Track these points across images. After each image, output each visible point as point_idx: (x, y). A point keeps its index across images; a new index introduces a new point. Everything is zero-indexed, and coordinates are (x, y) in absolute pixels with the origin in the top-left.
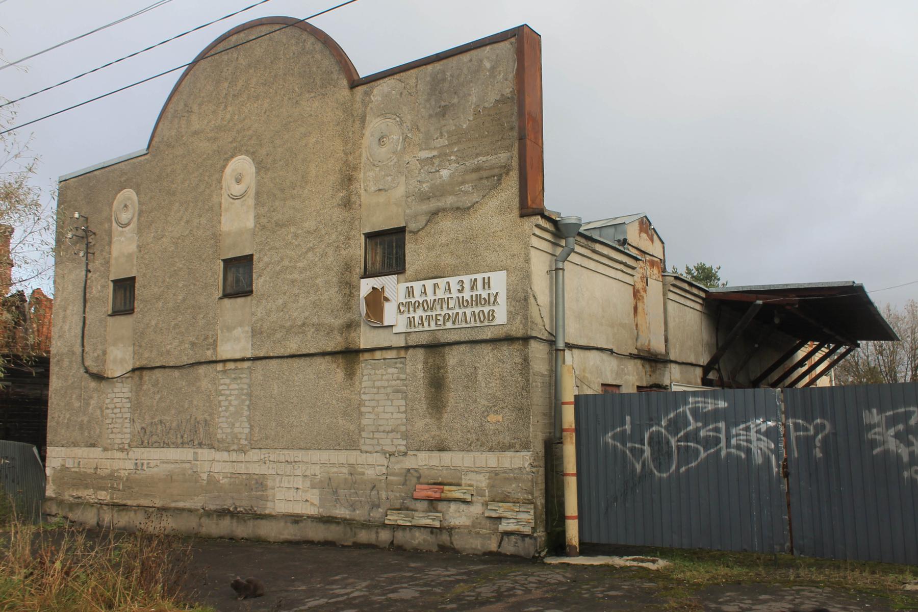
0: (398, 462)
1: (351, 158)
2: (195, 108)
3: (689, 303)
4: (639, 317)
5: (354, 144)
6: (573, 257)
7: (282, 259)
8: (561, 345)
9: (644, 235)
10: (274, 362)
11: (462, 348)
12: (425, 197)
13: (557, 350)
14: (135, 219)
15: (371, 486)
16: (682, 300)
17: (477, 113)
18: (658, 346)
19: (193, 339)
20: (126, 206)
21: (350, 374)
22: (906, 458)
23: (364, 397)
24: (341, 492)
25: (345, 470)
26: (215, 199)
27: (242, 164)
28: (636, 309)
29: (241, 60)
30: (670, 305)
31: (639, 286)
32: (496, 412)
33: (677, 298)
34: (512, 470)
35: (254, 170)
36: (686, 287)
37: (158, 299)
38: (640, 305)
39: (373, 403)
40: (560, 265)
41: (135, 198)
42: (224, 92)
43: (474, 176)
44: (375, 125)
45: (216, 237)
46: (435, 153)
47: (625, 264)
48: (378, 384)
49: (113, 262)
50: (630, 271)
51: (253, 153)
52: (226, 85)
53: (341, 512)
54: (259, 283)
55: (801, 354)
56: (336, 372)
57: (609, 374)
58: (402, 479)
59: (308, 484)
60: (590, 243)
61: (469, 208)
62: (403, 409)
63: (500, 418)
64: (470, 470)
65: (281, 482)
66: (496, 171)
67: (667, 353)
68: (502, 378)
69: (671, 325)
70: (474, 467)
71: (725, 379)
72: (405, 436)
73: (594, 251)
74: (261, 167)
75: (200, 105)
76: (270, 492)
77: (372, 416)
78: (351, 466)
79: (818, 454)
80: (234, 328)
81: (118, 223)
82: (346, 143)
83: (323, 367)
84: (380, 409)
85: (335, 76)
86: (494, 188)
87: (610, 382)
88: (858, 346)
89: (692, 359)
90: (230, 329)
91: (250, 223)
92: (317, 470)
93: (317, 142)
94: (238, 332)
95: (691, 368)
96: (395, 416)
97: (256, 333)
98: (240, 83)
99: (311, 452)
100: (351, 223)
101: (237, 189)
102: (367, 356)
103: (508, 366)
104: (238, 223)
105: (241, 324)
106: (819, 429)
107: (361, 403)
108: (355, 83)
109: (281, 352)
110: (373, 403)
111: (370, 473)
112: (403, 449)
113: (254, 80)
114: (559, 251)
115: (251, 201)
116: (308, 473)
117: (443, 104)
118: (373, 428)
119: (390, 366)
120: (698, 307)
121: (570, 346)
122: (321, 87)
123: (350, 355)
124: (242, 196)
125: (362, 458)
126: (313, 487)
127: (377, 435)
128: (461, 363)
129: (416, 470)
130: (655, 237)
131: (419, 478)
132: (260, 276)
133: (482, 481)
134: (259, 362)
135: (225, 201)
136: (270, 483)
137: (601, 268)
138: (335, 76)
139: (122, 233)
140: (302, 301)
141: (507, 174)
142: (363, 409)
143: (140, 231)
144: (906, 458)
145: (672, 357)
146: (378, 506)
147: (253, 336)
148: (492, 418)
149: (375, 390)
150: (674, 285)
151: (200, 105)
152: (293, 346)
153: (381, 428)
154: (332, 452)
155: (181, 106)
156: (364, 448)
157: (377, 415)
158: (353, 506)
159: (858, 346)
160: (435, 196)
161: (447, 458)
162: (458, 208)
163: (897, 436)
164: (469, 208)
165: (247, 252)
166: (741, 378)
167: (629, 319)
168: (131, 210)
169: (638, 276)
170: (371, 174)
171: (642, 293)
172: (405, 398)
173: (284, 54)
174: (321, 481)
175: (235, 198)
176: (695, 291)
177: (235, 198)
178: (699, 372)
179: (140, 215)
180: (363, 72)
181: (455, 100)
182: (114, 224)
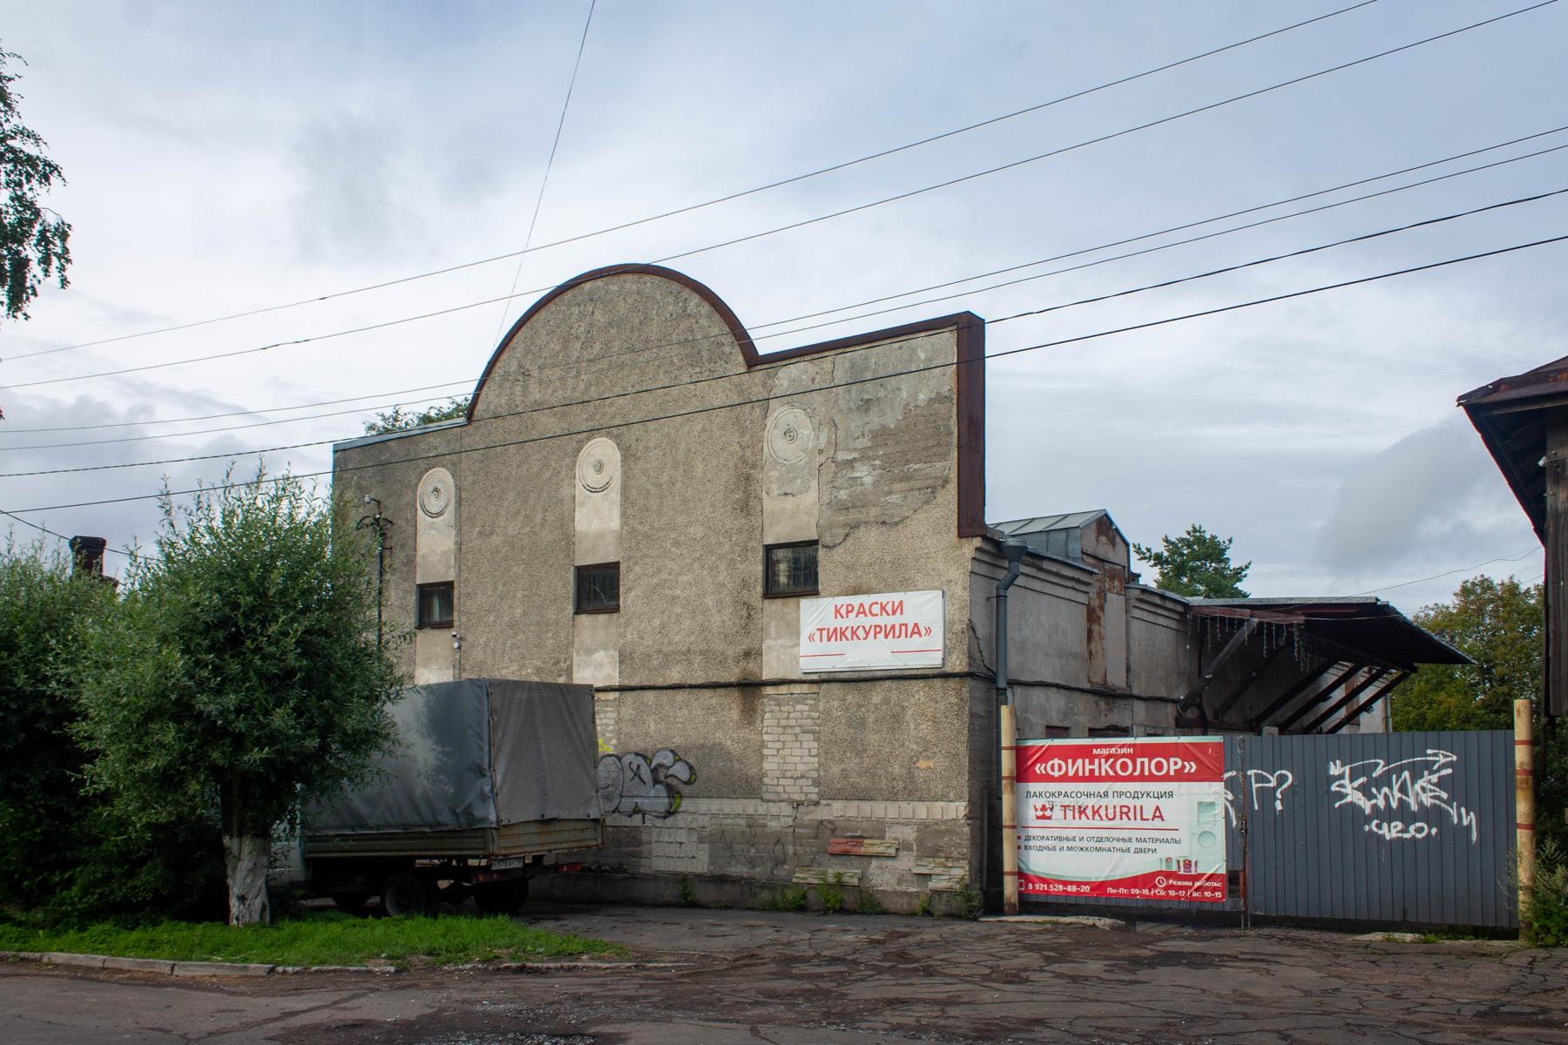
0: (807, 813)
1: (748, 453)
2: (535, 373)
3: (1161, 620)
4: (1093, 644)
5: (752, 436)
6: (1020, 581)
7: (659, 570)
8: (1002, 684)
9: (1103, 539)
10: (650, 695)
11: (887, 683)
12: (845, 508)
13: (998, 689)
14: (451, 508)
15: (774, 840)
16: (1151, 618)
17: (906, 413)
18: (1117, 679)
19: (538, 663)
20: (436, 490)
21: (750, 713)
22: (1368, 811)
23: (765, 737)
24: (737, 847)
25: (743, 822)
26: (565, 491)
27: (602, 449)
28: (1090, 633)
29: (598, 316)
30: (1136, 626)
31: (1095, 603)
32: (928, 758)
33: (1145, 615)
34: (945, 822)
35: (618, 456)
36: (1158, 601)
37: (489, 612)
38: (1095, 628)
39: (778, 745)
40: (1002, 593)
41: (451, 481)
42: (576, 354)
43: (904, 485)
44: (782, 415)
45: (568, 539)
46: (856, 455)
47: (1078, 581)
48: (784, 722)
49: (419, 560)
50: (1083, 588)
51: (618, 436)
52: (578, 345)
53: (738, 870)
54: (627, 599)
55: (1331, 677)
56: (730, 707)
57: (1054, 715)
58: (813, 832)
59: (695, 837)
60: (1037, 562)
61: (897, 524)
62: (814, 752)
63: (931, 764)
64: (895, 823)
65: (659, 835)
66: (930, 482)
67: (1129, 686)
68: (935, 720)
69: (1135, 650)
70: (901, 817)
71: (1209, 715)
72: (817, 782)
73: (1040, 569)
74: (628, 454)
75: (541, 368)
76: (645, 848)
77: (777, 760)
78: (750, 816)
79: (1279, 806)
80: (595, 651)
81: (426, 512)
82: (743, 434)
83: (714, 701)
84: (786, 752)
85: (727, 349)
86: (927, 502)
87: (1056, 723)
88: (1415, 670)
89: (1163, 693)
90: (589, 652)
91: (615, 523)
92: (703, 821)
93: (704, 430)
94: (600, 656)
95: (1162, 705)
96: (806, 759)
97: (624, 658)
98: (597, 346)
99: (699, 801)
100: (751, 530)
101: (595, 480)
102: (769, 690)
103: (941, 706)
104: (598, 523)
105: (604, 647)
106: (1282, 779)
107: (763, 745)
108: (753, 360)
109: (660, 682)
110: (778, 745)
111: (773, 825)
112: (814, 797)
113: (617, 343)
114: (1002, 574)
115: (615, 495)
116: (693, 825)
117: (866, 397)
118: (778, 774)
119: (798, 703)
120: (1173, 624)
121: (1013, 683)
122: (710, 360)
123: (750, 687)
124: (603, 489)
125: (762, 808)
126: (701, 840)
127: (782, 781)
128: (886, 701)
129: (830, 822)
130: (1118, 539)
131: (833, 831)
132: (630, 589)
133: (909, 834)
134: (628, 695)
135: (580, 492)
136: (645, 837)
137: (1048, 588)
138: (727, 349)
139: (431, 527)
140: (687, 624)
141: (943, 487)
142: (765, 751)
143: (459, 525)
144: (1368, 811)
145: (1135, 692)
146: (784, 862)
147: (621, 663)
148: (922, 764)
149: (780, 730)
150: (1140, 600)
151: (541, 368)
152: (675, 676)
153: (788, 774)
154: (726, 801)
155: (514, 367)
156: (766, 796)
157: (784, 757)
158: (752, 863)
159: (1415, 670)
160: (854, 507)
161: (867, 807)
162: (884, 523)
163: (1360, 788)
164: (897, 524)
165: (612, 559)
166: (1232, 717)
167: (1079, 647)
168: (443, 495)
169: (1093, 591)
170: (774, 474)
171: (1099, 612)
172: (817, 740)
173: (658, 315)
174: (711, 835)
175: (593, 490)
176: (1170, 605)
177: (593, 490)
178: (1171, 709)
179: (459, 501)
180: (763, 348)
181: (882, 394)
182: (420, 512)
